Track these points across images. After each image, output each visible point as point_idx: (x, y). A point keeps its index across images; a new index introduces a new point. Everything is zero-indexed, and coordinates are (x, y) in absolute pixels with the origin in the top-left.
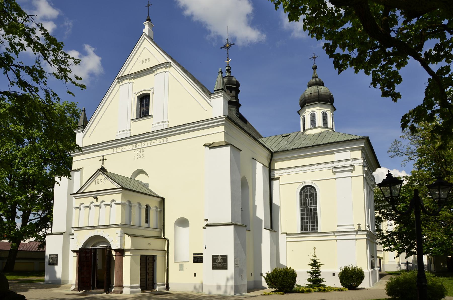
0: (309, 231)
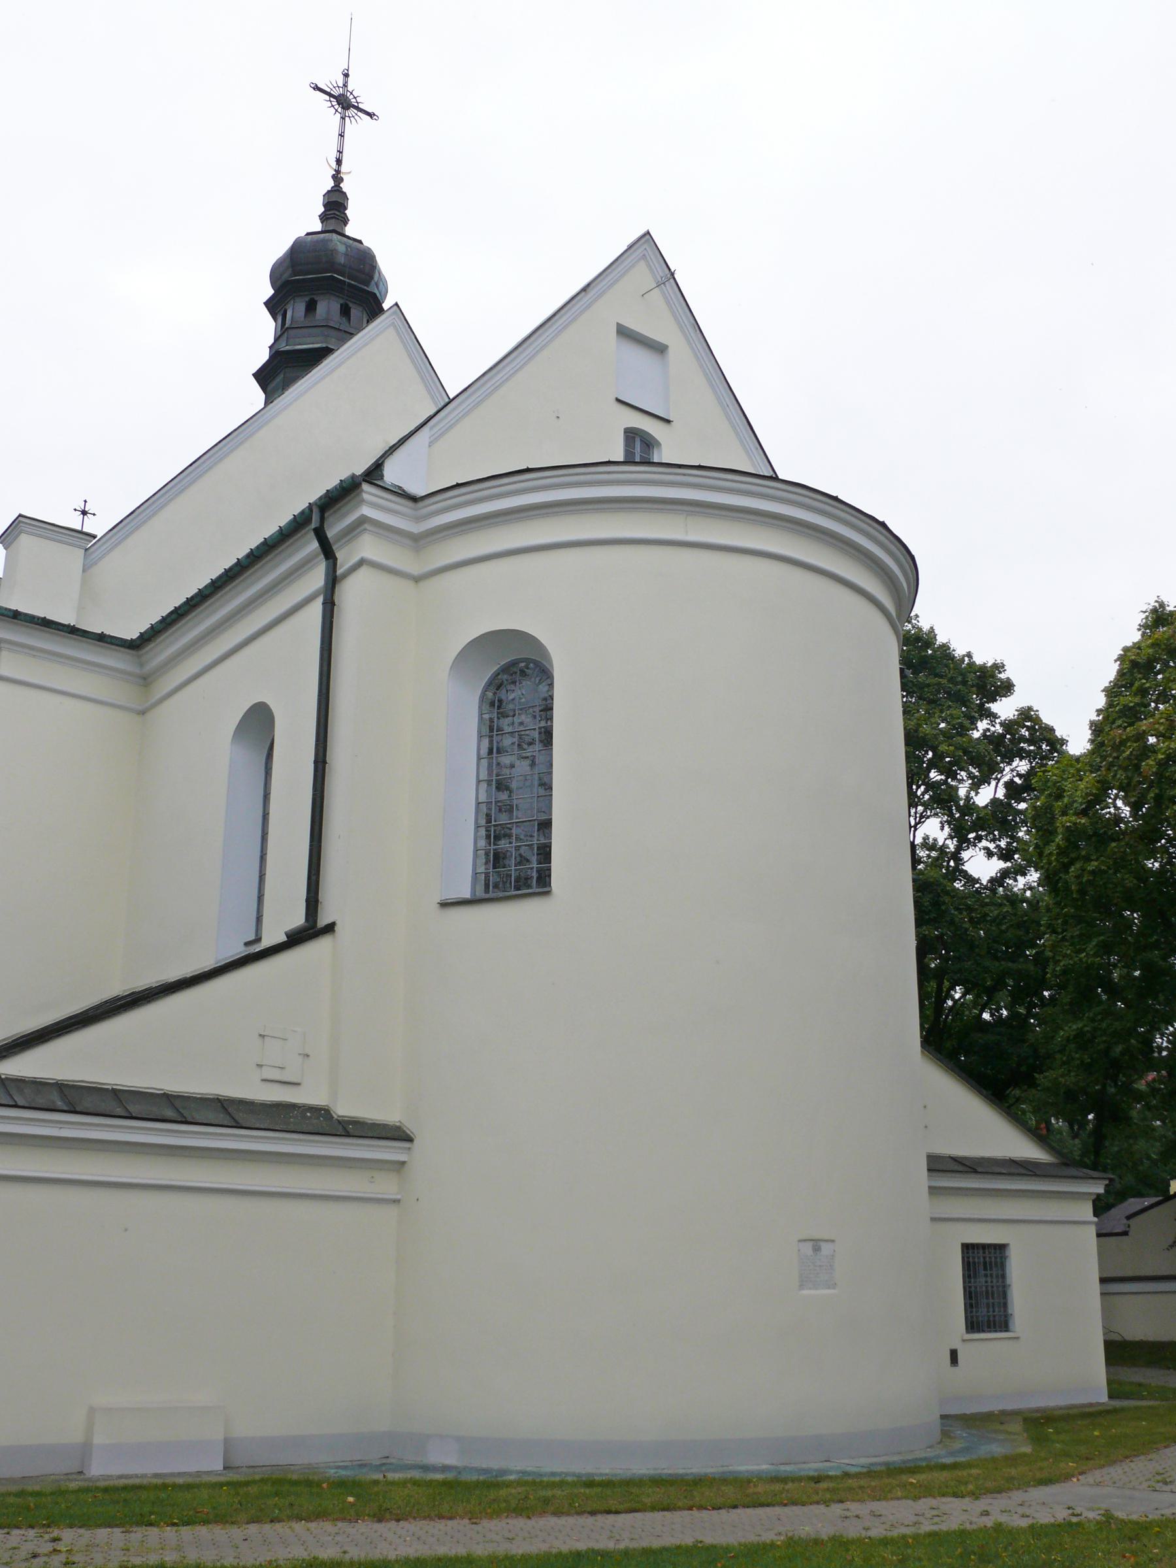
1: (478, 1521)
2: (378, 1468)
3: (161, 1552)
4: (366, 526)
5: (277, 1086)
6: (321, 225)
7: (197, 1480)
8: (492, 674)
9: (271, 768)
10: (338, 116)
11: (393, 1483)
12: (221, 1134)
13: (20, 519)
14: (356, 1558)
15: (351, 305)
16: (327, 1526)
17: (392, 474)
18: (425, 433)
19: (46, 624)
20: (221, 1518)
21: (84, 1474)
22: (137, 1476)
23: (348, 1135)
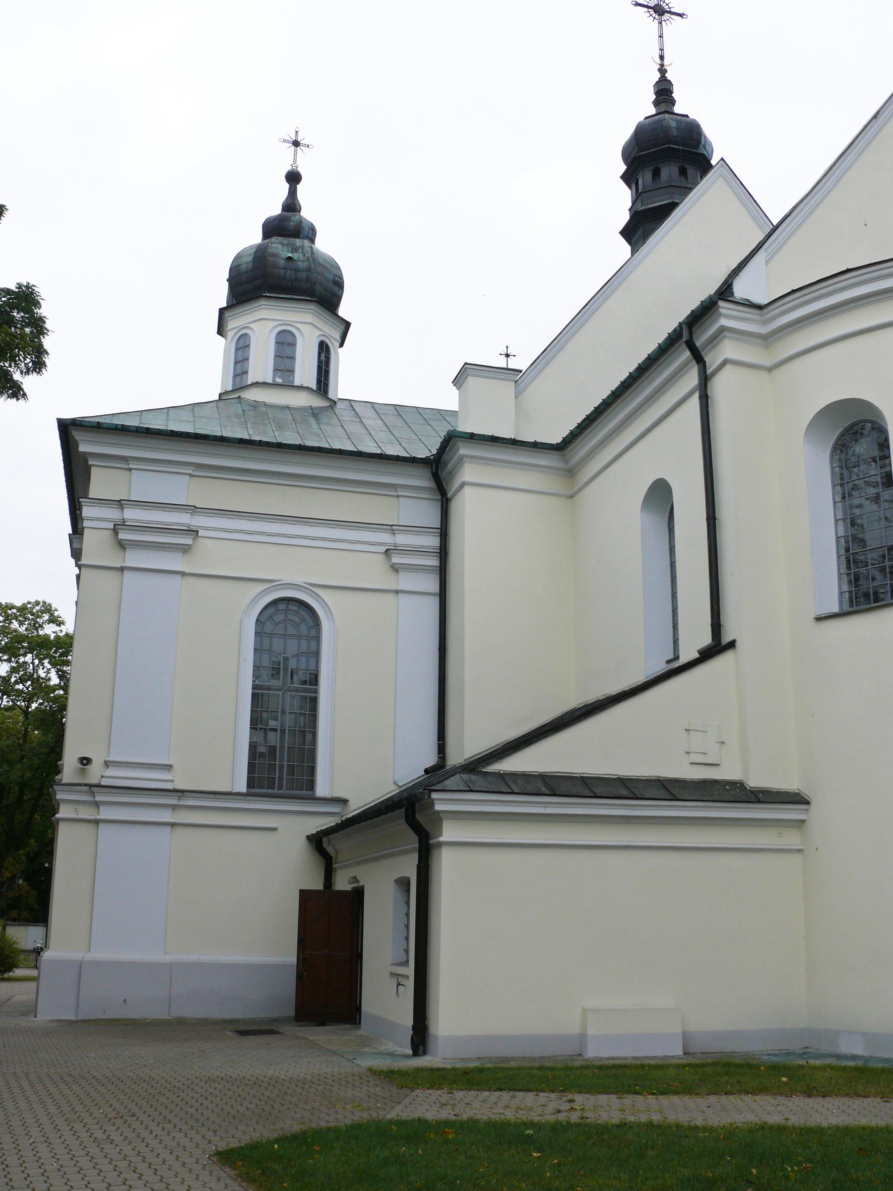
0: (276, 791)
1: (889, 1100)
2: (802, 1056)
3: (648, 1113)
4: (726, 334)
5: (702, 768)
6: (655, 109)
7: (666, 1062)
8: (838, 436)
9: (673, 527)
10: (656, 21)
11: (815, 1068)
12: (648, 806)
13: (466, 366)
14: (797, 1125)
15: (686, 166)
16: (770, 1099)
17: (740, 290)
18: (762, 254)
19: (494, 440)
20: (688, 1090)
21: (583, 1056)
22: (620, 1058)
23: (759, 801)
